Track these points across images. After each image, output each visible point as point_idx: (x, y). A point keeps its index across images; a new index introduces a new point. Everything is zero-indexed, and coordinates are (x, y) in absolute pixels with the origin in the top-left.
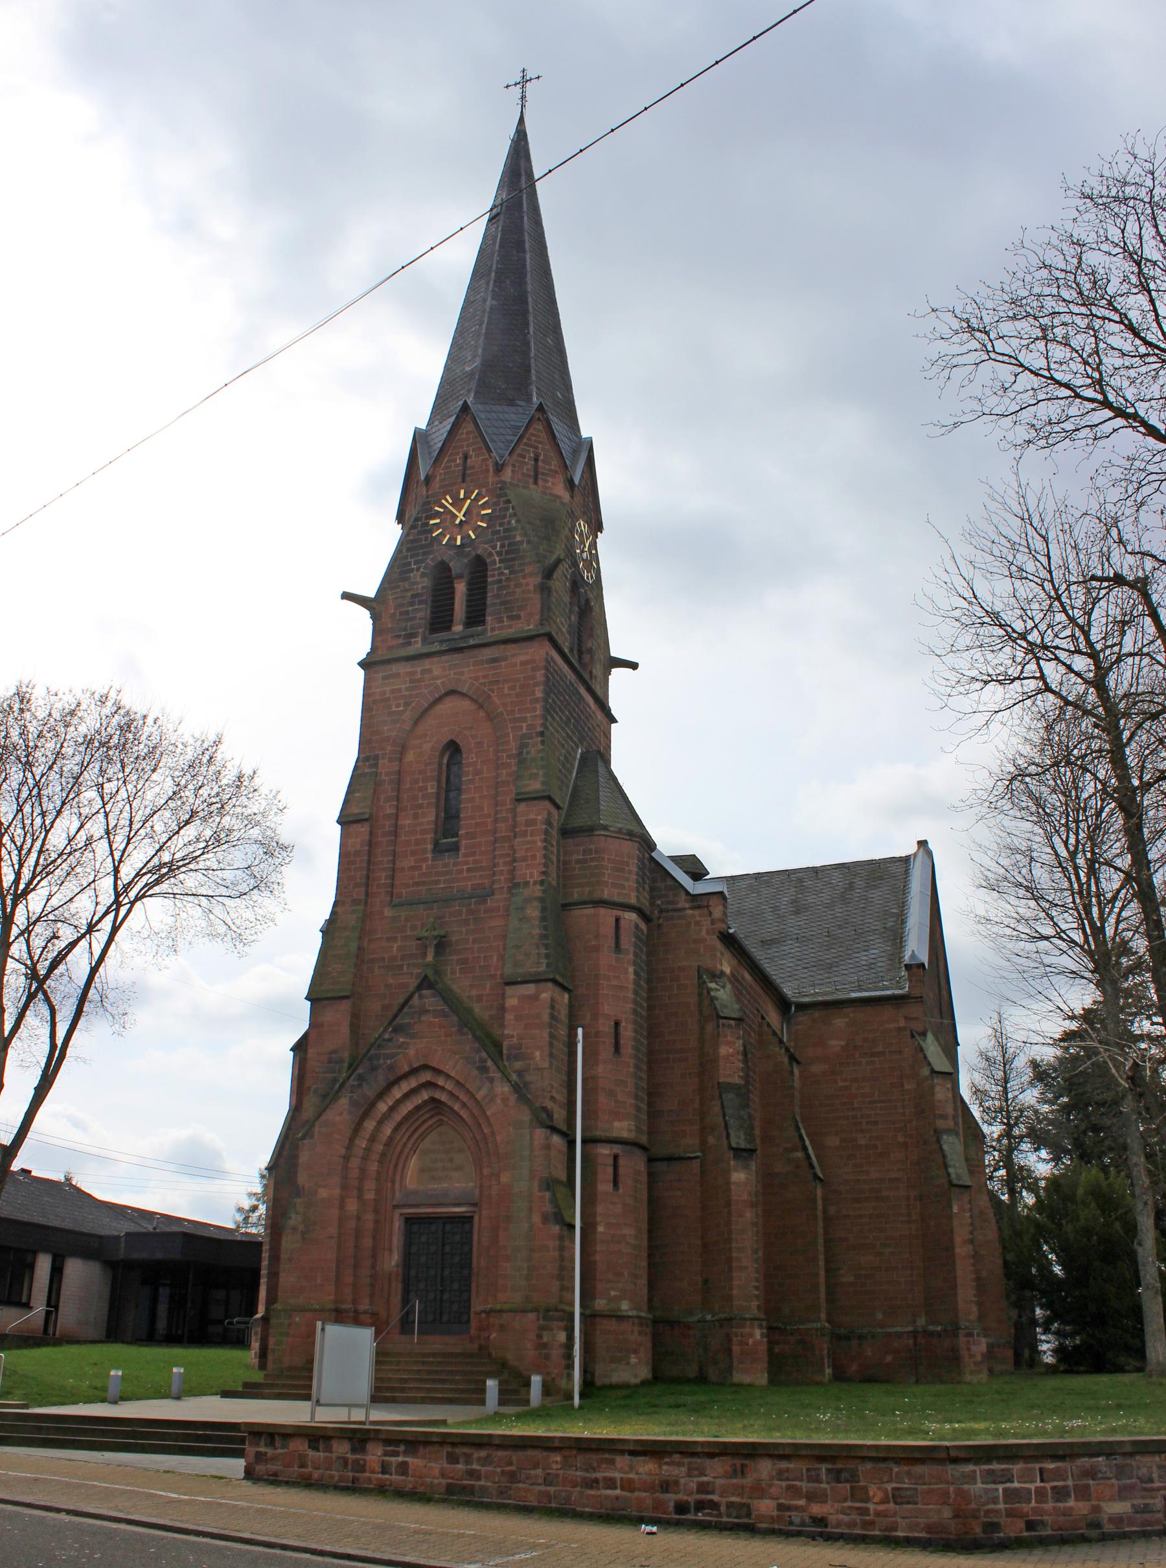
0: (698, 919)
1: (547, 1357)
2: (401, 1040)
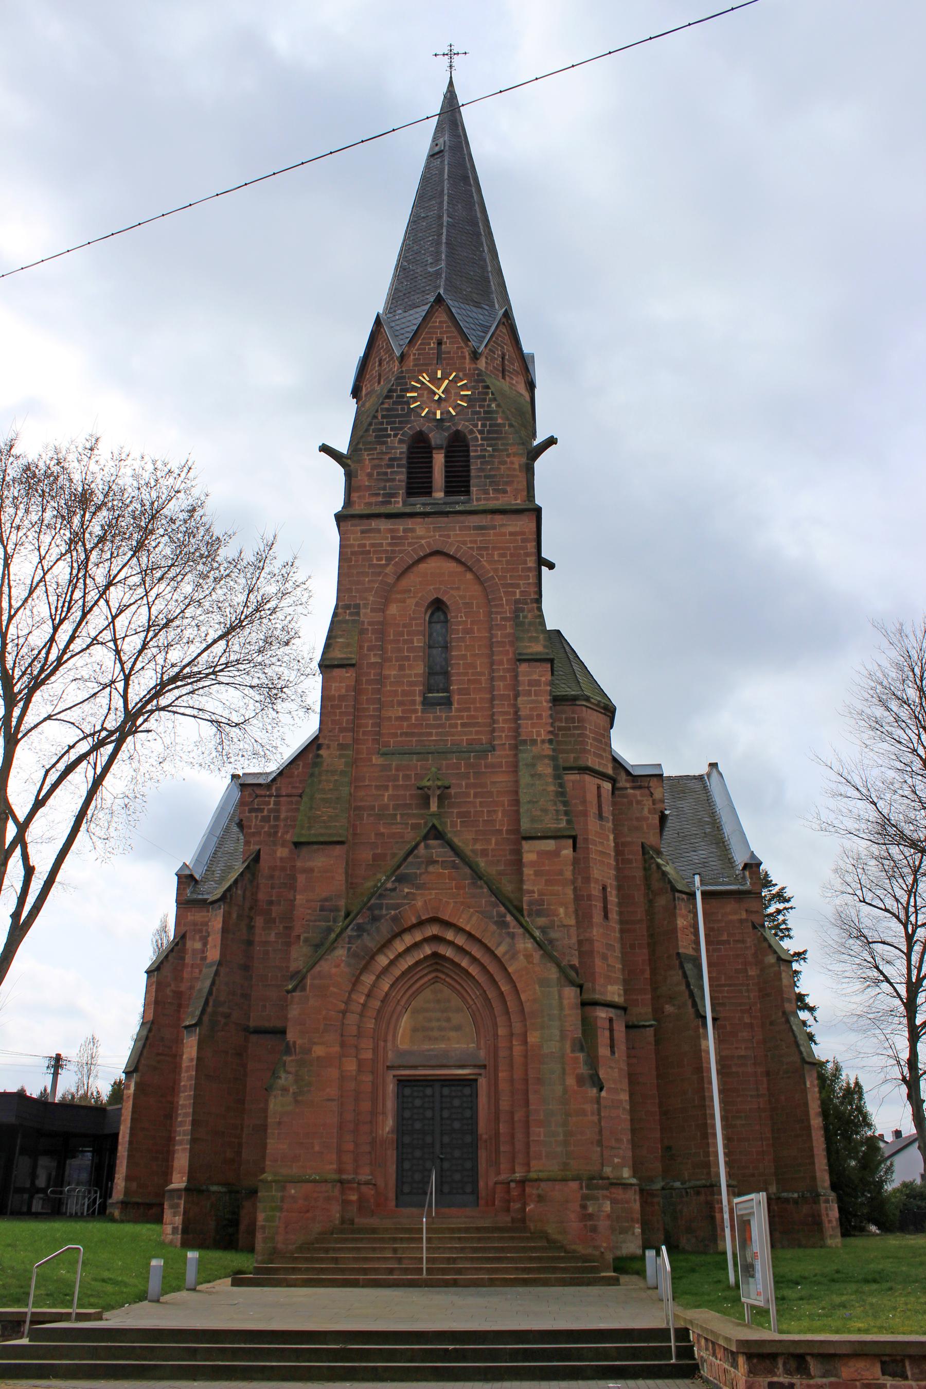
0: (639, 798)
1: (594, 1229)
2: (406, 890)
